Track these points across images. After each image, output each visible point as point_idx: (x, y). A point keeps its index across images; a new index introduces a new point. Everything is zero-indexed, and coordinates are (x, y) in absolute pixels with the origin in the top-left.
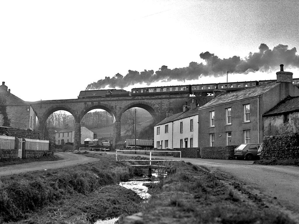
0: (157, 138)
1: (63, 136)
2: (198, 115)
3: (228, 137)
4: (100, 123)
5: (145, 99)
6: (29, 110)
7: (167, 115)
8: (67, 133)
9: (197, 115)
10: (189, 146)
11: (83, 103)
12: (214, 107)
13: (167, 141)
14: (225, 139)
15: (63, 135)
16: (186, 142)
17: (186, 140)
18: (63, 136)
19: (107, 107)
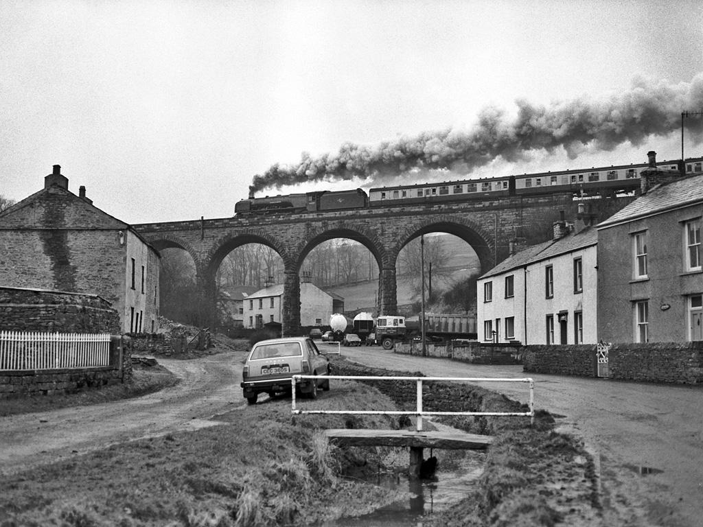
0: (485, 312)
1: (261, 307)
2: (596, 247)
3: (691, 311)
4: (353, 274)
5: (458, 210)
6: (125, 240)
7: (511, 249)
8: (269, 300)
9: (593, 245)
10: (571, 341)
11: (302, 226)
12: (645, 220)
13: (510, 321)
14: (683, 316)
15: (261, 304)
16: (564, 324)
17: (563, 318)
18: (261, 307)
19: (360, 231)
